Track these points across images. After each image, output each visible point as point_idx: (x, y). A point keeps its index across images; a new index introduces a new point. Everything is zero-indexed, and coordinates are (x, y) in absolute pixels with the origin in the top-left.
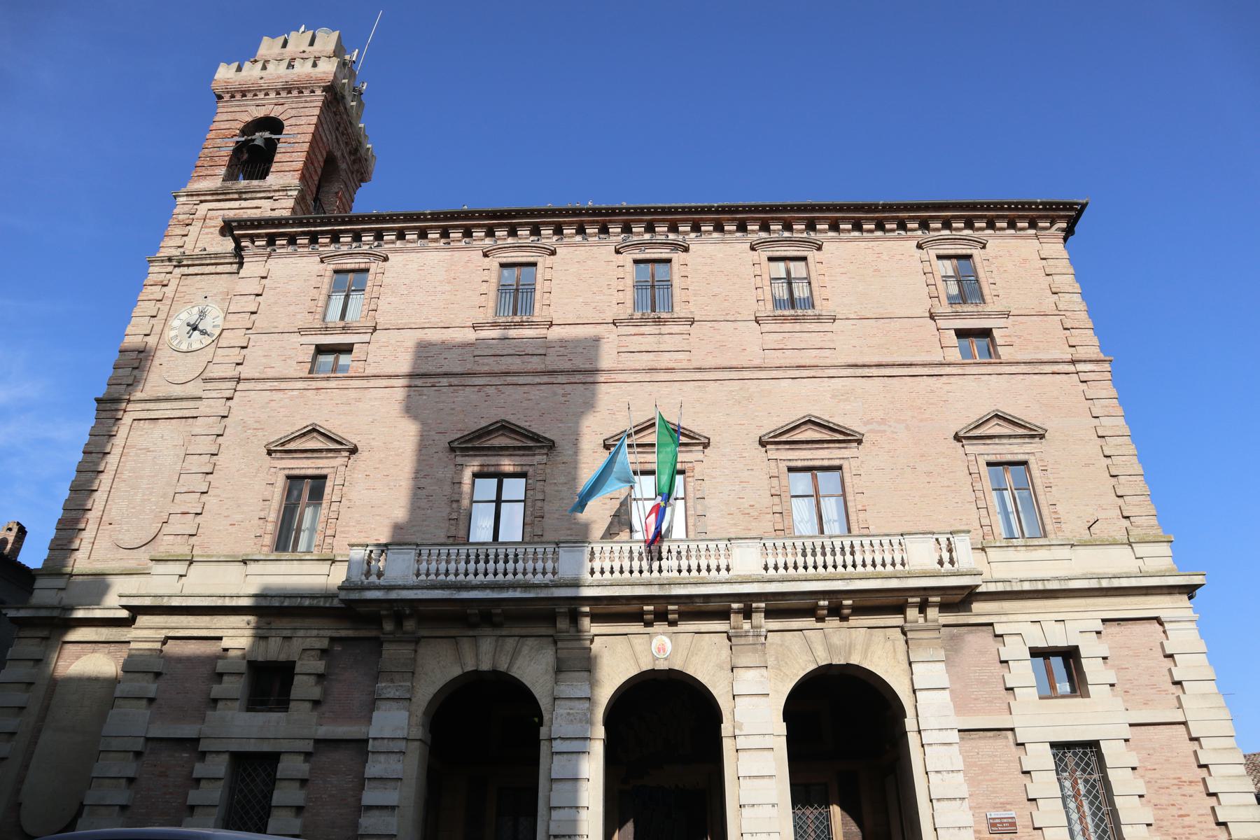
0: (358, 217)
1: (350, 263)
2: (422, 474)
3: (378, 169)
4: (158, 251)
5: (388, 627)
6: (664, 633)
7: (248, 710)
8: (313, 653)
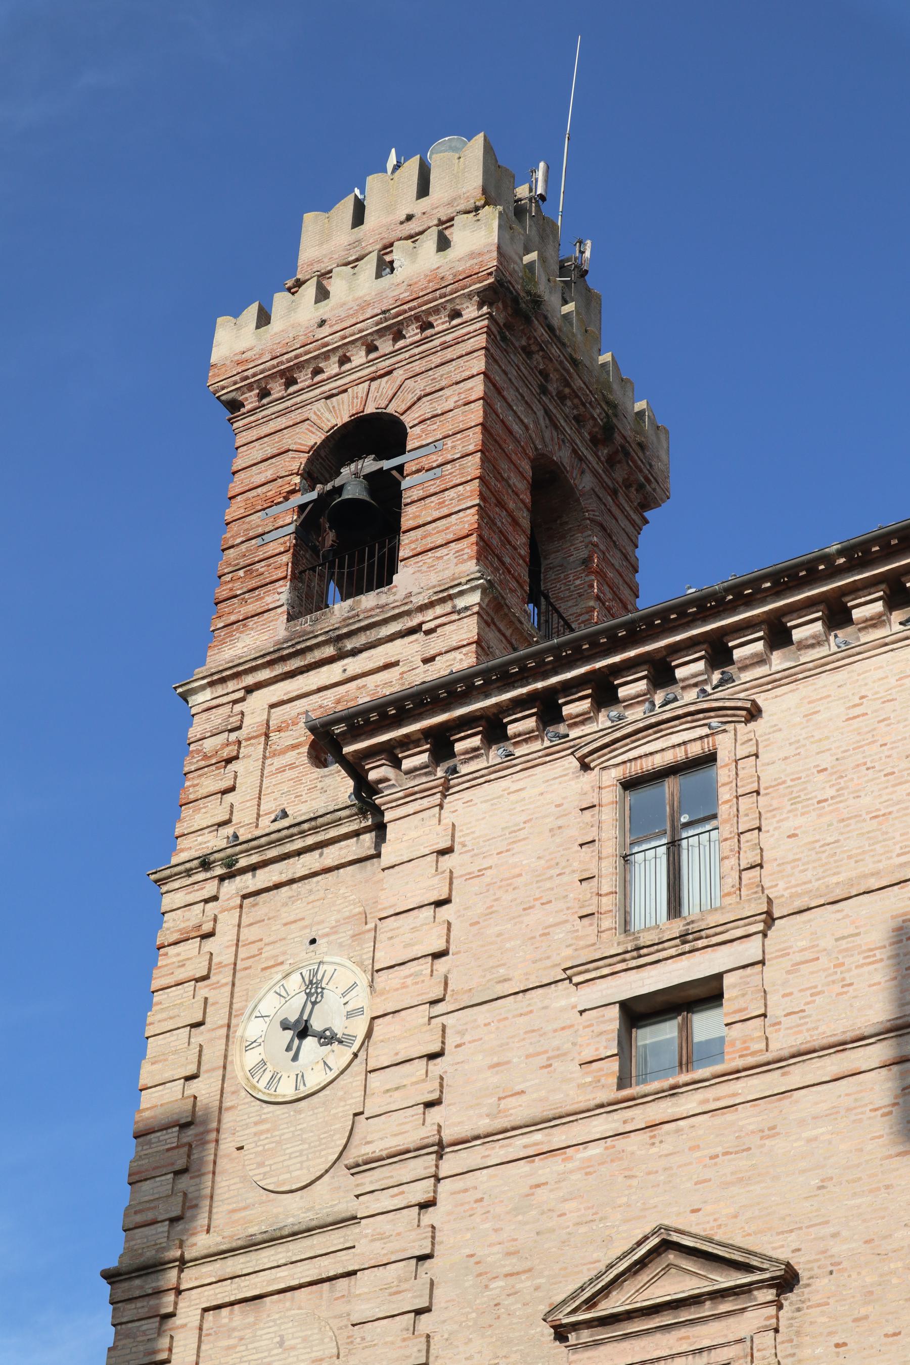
0: (663, 613)
1: (660, 751)
3: (680, 463)
4: (172, 849)
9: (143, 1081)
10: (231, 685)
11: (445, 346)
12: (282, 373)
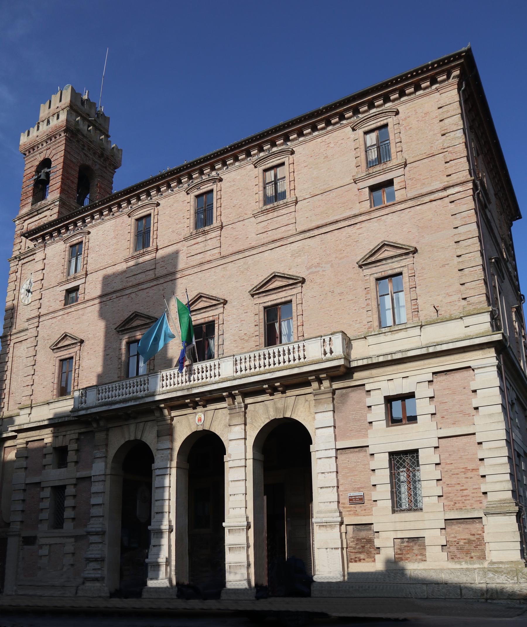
2: (108, 347)
4: (12, 254)
5: (95, 425)
6: (201, 412)
7: (59, 468)
8: (73, 441)
9: (7, 301)
10: (22, 220)
11: (59, 143)
12: (32, 148)
